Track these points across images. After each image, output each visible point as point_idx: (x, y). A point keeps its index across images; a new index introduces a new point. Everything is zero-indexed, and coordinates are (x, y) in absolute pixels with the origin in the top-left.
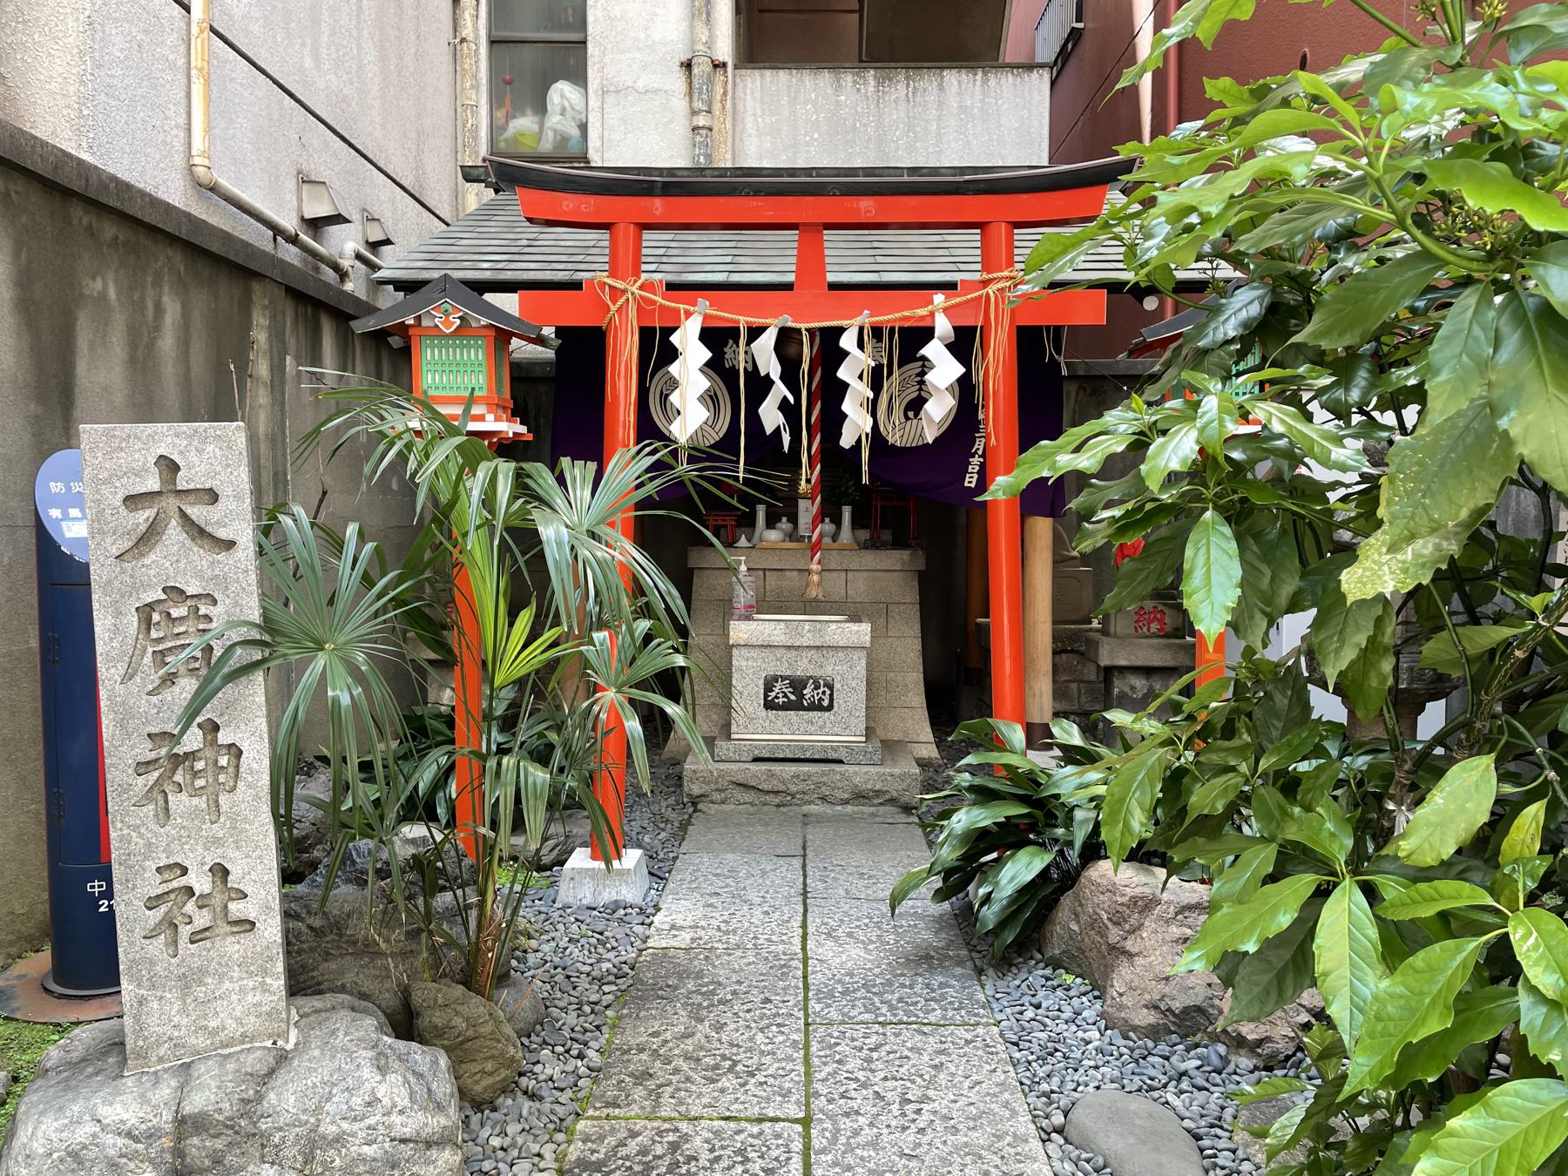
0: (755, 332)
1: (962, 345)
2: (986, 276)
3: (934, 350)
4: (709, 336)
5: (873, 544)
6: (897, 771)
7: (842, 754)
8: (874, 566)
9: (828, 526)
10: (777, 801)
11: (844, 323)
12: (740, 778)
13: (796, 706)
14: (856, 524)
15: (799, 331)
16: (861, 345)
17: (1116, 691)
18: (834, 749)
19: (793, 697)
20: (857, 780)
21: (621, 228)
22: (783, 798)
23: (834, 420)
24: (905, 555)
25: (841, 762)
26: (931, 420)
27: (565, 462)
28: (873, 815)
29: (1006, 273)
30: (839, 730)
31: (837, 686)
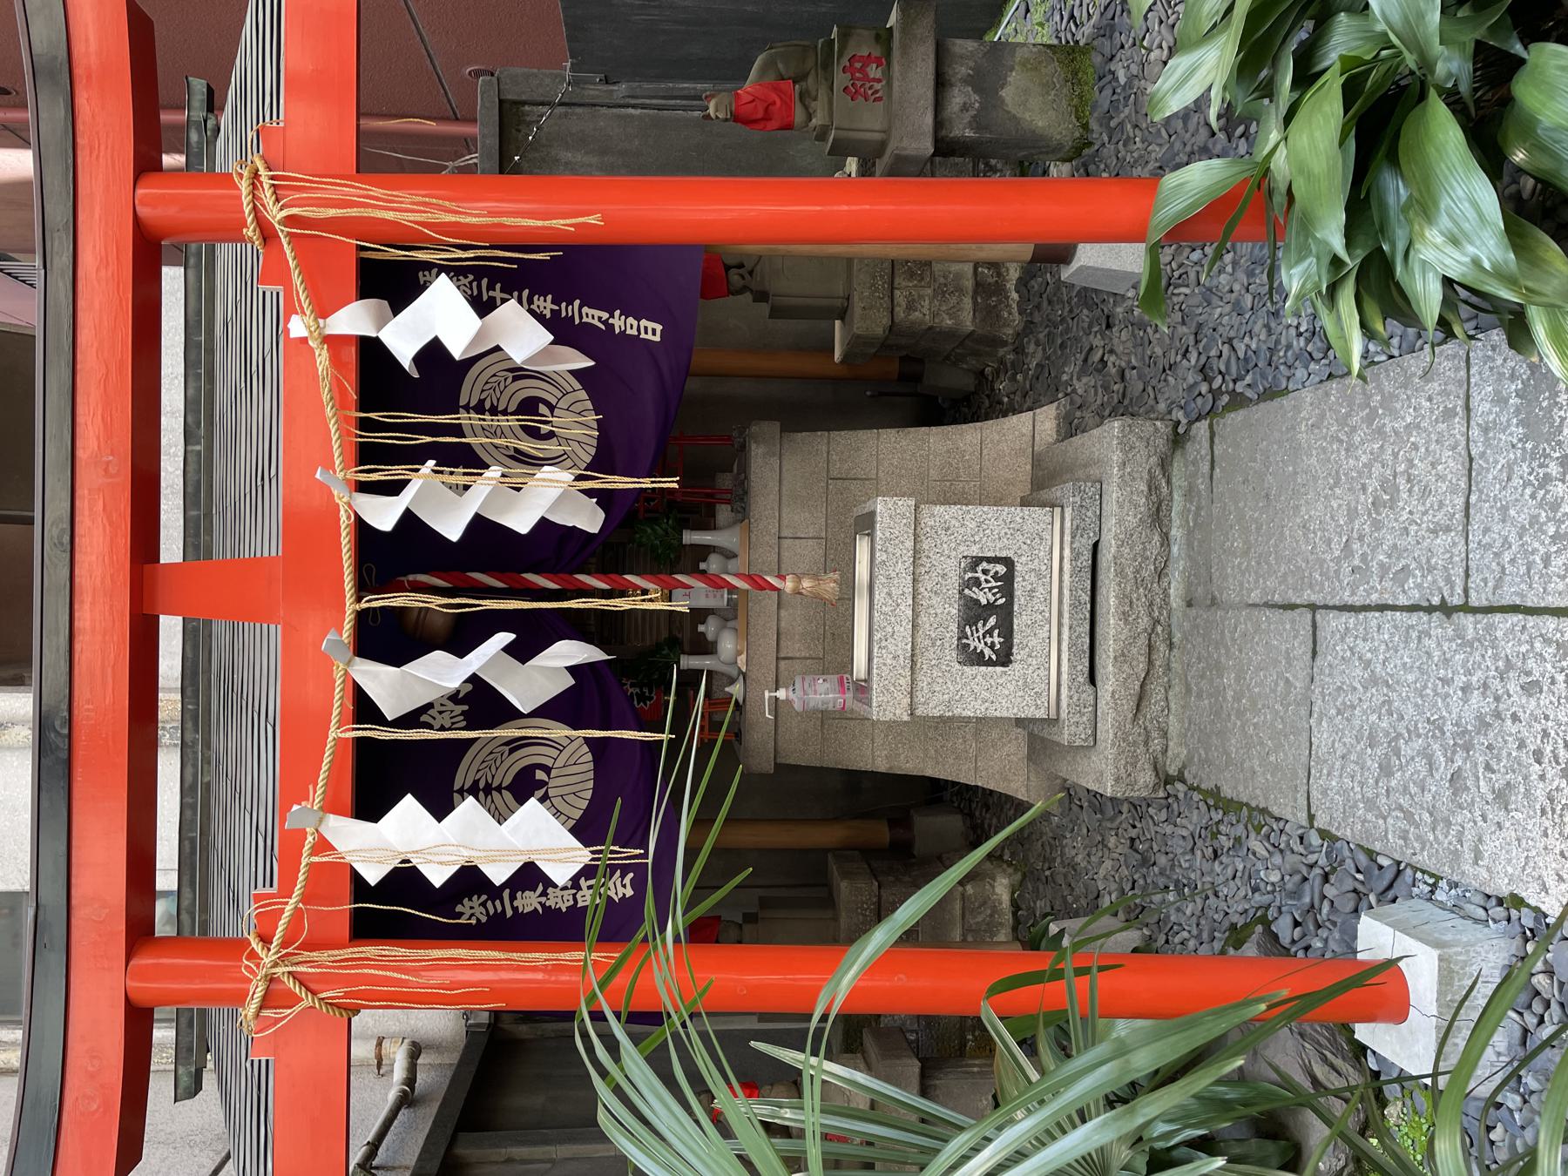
0: (364, 709)
1: (394, 284)
2: (250, 231)
3: (403, 338)
4: (370, 807)
5: (740, 499)
6: (1116, 457)
7: (1086, 543)
8: (774, 497)
9: (713, 565)
10: (1162, 647)
11: (345, 521)
12: (1128, 706)
13: (1006, 615)
14: (708, 524)
15: (361, 616)
16: (393, 488)
17: (968, 133)
18: (1076, 556)
19: (992, 621)
20: (1132, 520)
21: (144, 988)
22: (1156, 640)
23: (551, 539)
24: (757, 452)
25: (1096, 545)
26: (542, 355)
27: (703, 566)
28: (1189, 494)
29: (244, 186)
30: (1042, 547)
31: (975, 551)
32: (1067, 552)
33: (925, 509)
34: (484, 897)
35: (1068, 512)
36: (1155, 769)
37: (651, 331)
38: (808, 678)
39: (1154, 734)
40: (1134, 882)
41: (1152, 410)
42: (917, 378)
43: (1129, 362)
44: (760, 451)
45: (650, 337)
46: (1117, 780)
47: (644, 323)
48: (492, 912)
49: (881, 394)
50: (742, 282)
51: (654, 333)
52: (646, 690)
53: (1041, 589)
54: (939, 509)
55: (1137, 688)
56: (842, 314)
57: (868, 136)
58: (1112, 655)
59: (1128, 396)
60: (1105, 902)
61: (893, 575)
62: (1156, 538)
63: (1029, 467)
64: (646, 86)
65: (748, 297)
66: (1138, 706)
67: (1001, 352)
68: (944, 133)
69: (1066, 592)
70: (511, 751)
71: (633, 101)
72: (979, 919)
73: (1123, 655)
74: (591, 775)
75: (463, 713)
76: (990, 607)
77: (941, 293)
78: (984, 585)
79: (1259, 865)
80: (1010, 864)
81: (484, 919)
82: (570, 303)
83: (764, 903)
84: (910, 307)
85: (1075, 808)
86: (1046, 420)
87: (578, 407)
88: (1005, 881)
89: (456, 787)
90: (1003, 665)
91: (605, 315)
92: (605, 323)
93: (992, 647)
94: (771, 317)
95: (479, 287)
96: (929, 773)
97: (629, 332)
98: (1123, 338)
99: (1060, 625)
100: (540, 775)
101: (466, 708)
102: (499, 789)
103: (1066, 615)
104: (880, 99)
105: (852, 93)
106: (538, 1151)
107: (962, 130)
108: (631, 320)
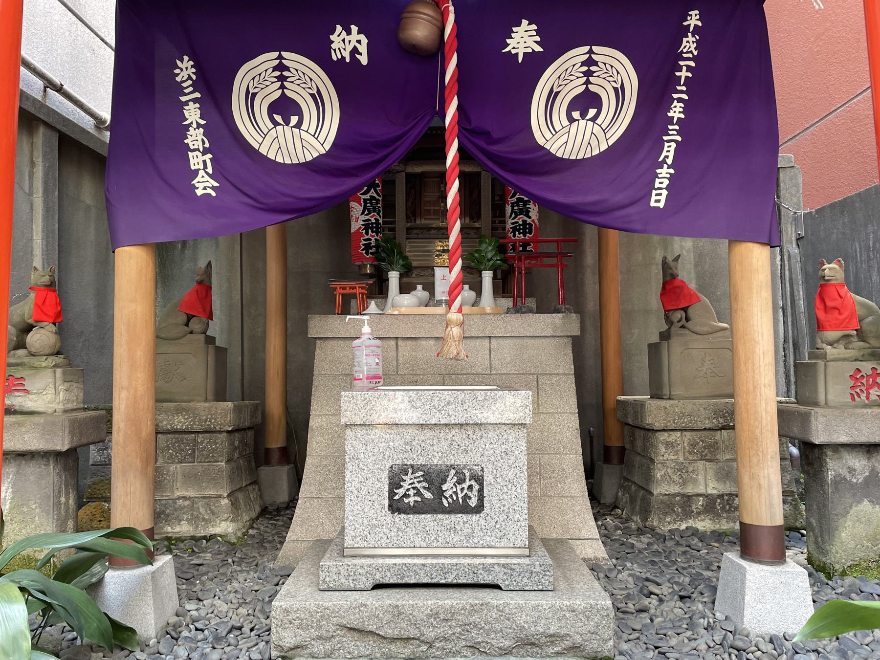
6: (579, 604)
9: (467, 293)
13: (434, 507)
17: (831, 474)
18: (487, 569)
19: (428, 495)
20: (521, 619)
25: (497, 587)
31: (488, 478)
32: (490, 561)
33: (522, 433)
34: (194, 77)
35: (526, 561)
36: (297, 647)
37: (659, 199)
38: (379, 351)
39: (328, 646)
40: (202, 631)
41: (620, 638)
42: (607, 460)
43: (657, 617)
44: (557, 321)
45: (654, 198)
46: (287, 611)
47: (665, 193)
48: (184, 85)
49: (591, 437)
50: (675, 320)
51: (658, 201)
52: (374, 250)
53: (457, 538)
54: (523, 445)
55: (370, 628)
56: (656, 395)
57: (821, 389)
58: (400, 603)
59: (626, 616)
60: (191, 606)
61: (466, 406)
62: (507, 643)
63: (554, 536)
64: (798, 265)
65: (665, 327)
66: (354, 629)
67: (637, 518)
68: (829, 453)
69: (454, 561)
70: (312, 95)
71: (786, 258)
72: (202, 510)
73: (400, 614)
74: (295, 161)
75: (343, 58)
76: (440, 493)
77: (681, 469)
78: (459, 487)
79: (690, 570)
80: (244, 534)
81: (178, 79)
82: (679, 133)
83: (221, 353)
84: (668, 445)
85: (276, 580)
86: (596, 550)
87: (594, 143)
88: (230, 530)
89: (284, 54)
90: (390, 506)
91: (669, 161)
92: (664, 161)
93: (406, 495)
94: (650, 345)
95: (688, 59)
96: (309, 460)
97: (657, 181)
98: (675, 610)
99: (426, 556)
100: (294, 120)
101: (348, 60)
102: (282, 87)
103: (435, 561)
104: (853, 399)
105: (856, 376)
106: (39, 185)
107: (834, 468)
108: (666, 182)
